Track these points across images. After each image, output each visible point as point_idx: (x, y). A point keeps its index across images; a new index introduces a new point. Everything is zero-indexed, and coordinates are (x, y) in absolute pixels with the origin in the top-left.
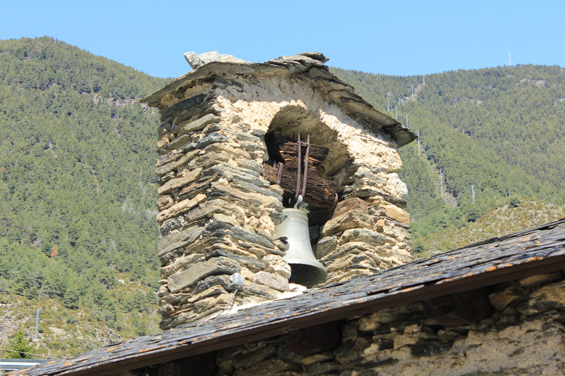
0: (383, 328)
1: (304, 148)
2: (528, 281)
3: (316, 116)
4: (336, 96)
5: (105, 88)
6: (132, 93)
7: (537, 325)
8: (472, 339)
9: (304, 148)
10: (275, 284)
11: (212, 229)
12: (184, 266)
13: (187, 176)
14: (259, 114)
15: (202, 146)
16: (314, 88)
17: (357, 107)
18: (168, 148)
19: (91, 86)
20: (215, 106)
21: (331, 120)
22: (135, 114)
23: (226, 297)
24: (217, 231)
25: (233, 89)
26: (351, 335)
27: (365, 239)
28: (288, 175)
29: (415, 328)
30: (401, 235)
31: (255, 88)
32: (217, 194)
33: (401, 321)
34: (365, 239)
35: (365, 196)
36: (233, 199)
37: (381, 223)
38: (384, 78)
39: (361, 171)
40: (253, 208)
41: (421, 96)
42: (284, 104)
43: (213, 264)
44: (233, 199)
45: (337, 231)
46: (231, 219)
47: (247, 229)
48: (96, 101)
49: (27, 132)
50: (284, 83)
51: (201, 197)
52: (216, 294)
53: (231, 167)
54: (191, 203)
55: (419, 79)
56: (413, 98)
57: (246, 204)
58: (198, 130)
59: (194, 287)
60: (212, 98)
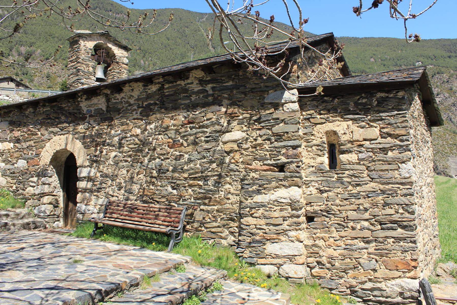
0: (81, 95)
1: (103, 52)
2: (102, 89)
3: (106, 44)
4: (112, 40)
5: (113, 10)
6: (121, 12)
7: (102, 96)
8: (93, 98)
9: (103, 52)
10: (92, 82)
11: (77, 70)
12: (72, 78)
13: (74, 58)
14: (91, 44)
15: (76, 52)
16: (106, 38)
17: (117, 43)
18: (70, 51)
19: (109, 10)
20: (80, 43)
21: (110, 45)
22: (122, 19)
23: (79, 85)
24: (78, 71)
25: (84, 39)
26: (77, 96)
27: (116, 72)
28: (99, 58)
29: (85, 96)
30: (126, 71)
31: (90, 38)
32: (79, 63)
33: (84, 94)
34: (116, 72)
35: (117, 63)
36: (82, 64)
37: (121, 69)
38: (196, 13)
39: (117, 57)
40: (88, 66)
41: (207, 19)
42: (98, 42)
43: (77, 78)
44: (82, 64)
45: (110, 70)
46: (82, 68)
47: (86, 70)
48: (110, 14)
49: (90, 23)
50: (98, 37)
51: (76, 63)
52: (77, 84)
53: (83, 57)
54: (73, 64)
55: (206, 14)
56: (204, 19)
57: (86, 65)
58: (76, 48)
59: (74, 82)
60: (79, 41)
